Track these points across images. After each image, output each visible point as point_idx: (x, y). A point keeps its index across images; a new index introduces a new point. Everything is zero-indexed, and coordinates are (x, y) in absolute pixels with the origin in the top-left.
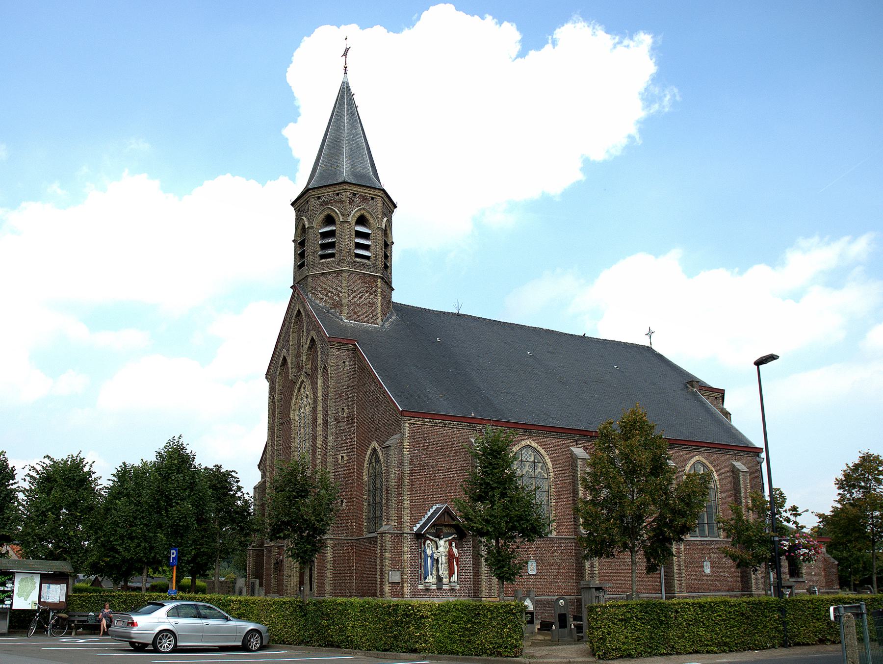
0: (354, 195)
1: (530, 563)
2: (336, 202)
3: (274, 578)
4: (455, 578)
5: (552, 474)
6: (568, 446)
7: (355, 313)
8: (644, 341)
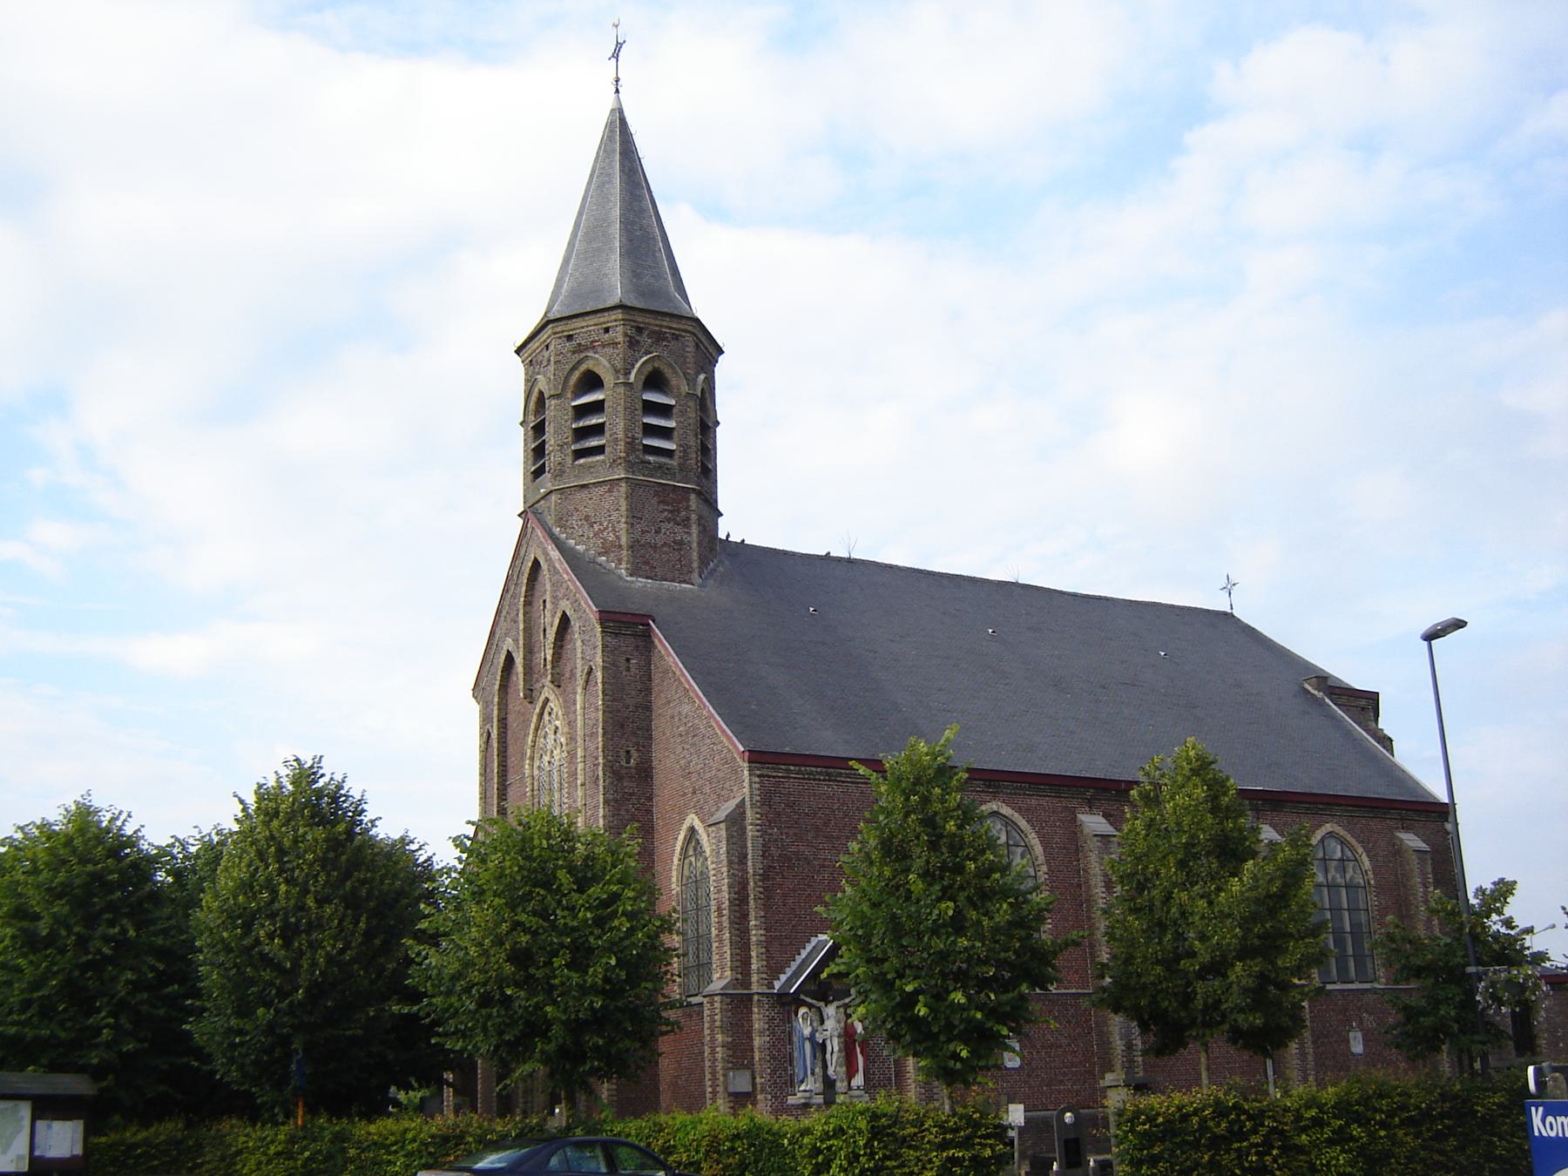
0: (639, 330)
5: (1044, 868)
7: (646, 563)
8: (1219, 604)
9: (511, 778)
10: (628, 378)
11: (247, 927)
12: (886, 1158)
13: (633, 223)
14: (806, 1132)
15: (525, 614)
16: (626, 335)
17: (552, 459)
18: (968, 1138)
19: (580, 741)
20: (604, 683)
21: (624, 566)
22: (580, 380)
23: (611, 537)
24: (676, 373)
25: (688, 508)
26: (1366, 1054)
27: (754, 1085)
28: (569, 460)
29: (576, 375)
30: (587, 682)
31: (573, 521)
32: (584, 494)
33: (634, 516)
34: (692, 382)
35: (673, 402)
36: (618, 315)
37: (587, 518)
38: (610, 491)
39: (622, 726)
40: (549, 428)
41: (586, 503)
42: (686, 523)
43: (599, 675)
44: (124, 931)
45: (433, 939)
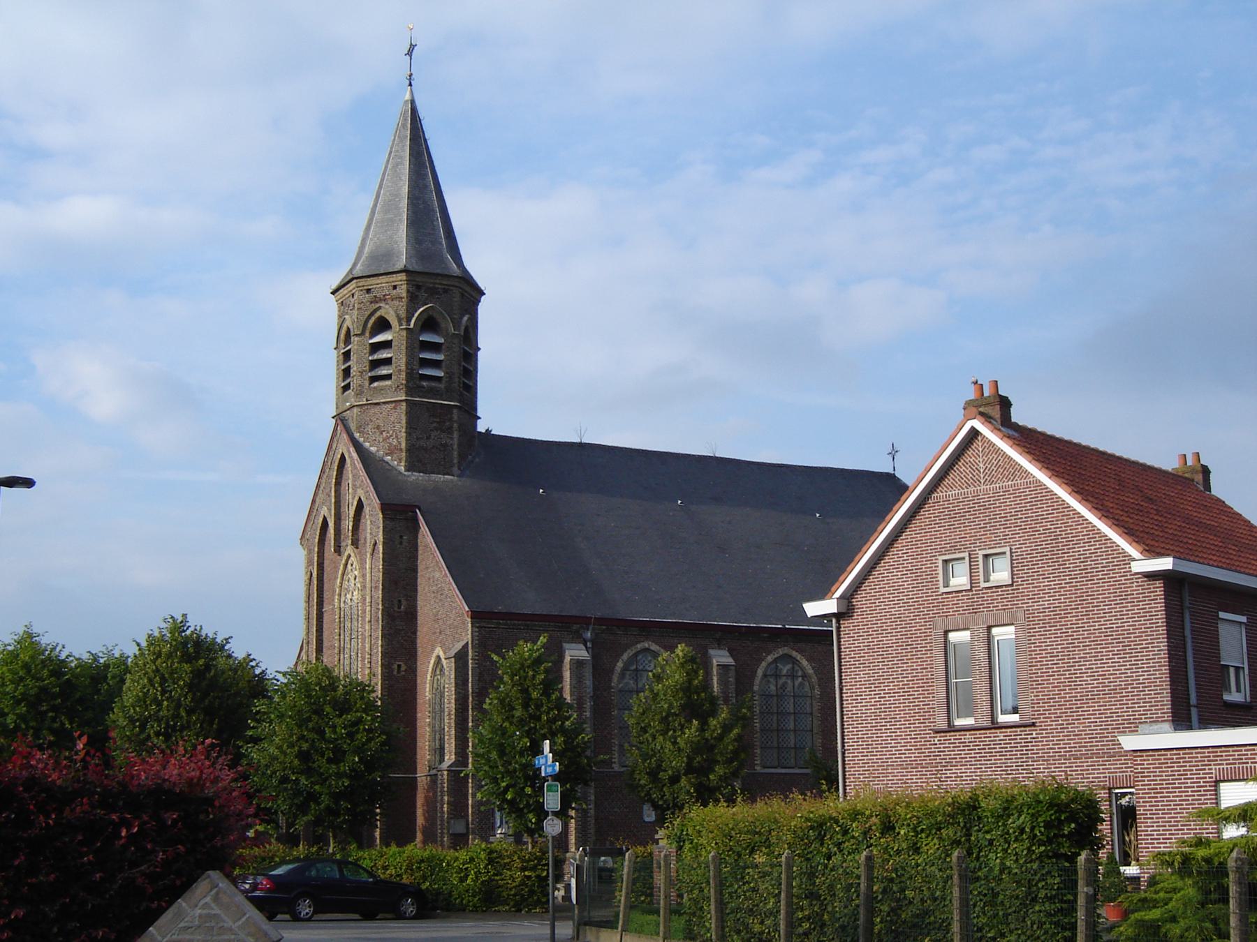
0: (418, 287)
3: (690, 850)
9: (326, 608)
10: (423, 313)
11: (143, 727)
12: (495, 875)
13: (418, 198)
14: (456, 859)
17: (355, 381)
18: (535, 866)
19: (368, 591)
22: (375, 323)
25: (451, 419)
27: (467, 828)
28: (367, 383)
29: (373, 319)
31: (369, 429)
33: (411, 427)
34: (456, 325)
35: (442, 341)
40: (353, 357)
42: (449, 430)
44: (63, 724)
45: (256, 740)
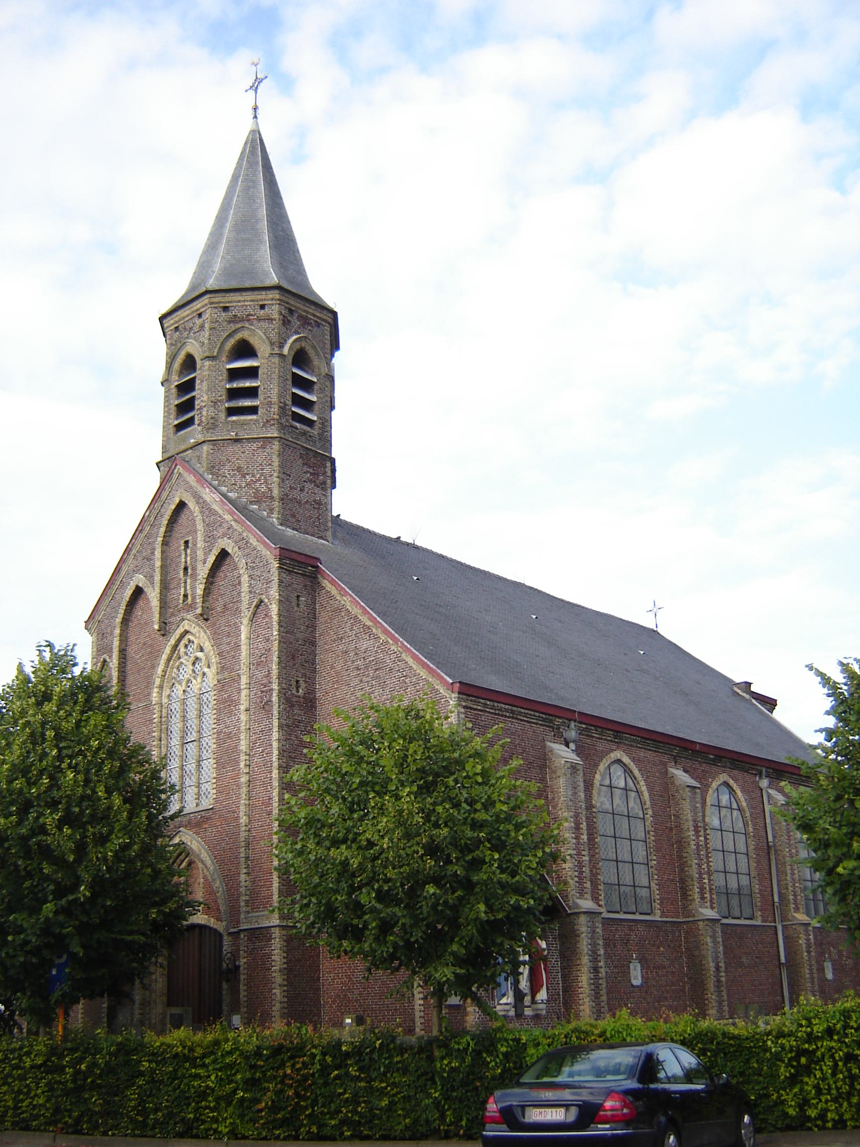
0: (291, 311)
1: (632, 966)
2: (259, 320)
4: (542, 995)
5: (650, 812)
6: (665, 765)
7: (294, 516)
10: (257, 357)
15: (163, 552)
16: (281, 314)
20: (280, 615)
21: (275, 515)
23: (264, 489)
24: (318, 354)
26: (834, 980)
28: (222, 416)
29: (232, 342)
30: (254, 614)
31: (226, 470)
32: (237, 447)
33: (285, 474)
36: (275, 294)
37: (239, 469)
38: (263, 447)
39: (293, 658)
41: (240, 455)
43: (274, 609)
